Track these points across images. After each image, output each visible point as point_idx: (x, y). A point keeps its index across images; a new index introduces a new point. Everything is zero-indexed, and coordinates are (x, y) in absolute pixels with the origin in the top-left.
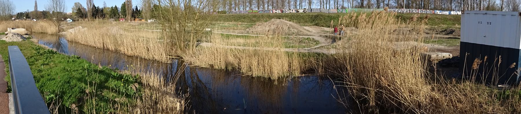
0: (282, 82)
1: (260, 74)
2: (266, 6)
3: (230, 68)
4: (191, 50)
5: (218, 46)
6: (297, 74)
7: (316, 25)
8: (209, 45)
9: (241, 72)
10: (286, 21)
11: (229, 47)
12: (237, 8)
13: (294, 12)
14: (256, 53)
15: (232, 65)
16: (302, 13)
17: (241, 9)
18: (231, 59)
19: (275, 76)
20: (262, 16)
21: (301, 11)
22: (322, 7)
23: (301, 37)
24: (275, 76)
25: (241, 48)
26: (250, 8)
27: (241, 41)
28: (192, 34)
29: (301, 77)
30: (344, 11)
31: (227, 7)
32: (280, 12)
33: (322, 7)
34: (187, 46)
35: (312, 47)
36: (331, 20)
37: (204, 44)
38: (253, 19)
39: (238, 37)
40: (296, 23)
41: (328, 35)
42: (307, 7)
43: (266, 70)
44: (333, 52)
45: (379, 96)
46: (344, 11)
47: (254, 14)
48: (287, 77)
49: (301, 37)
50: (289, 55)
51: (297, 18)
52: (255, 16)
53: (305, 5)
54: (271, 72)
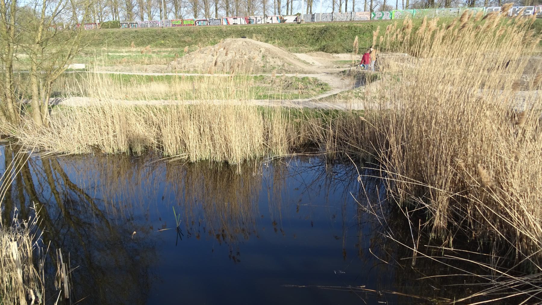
0: (251, 169)
1: (205, 155)
2: (212, 9)
3: (139, 149)
4: (38, 117)
5: (105, 102)
6: (281, 152)
7: (323, 49)
8: (83, 101)
9: (166, 154)
10: (259, 43)
11: (131, 103)
12: (145, 16)
13: (275, 21)
14: (193, 113)
15: (143, 141)
16: (291, 25)
17: (156, 18)
18: (140, 129)
19: (236, 158)
20: (205, 31)
21: (290, 19)
22: (337, 9)
23: (290, 75)
24: (236, 158)
25: (158, 104)
26: (176, 14)
27: (160, 88)
28: (34, 80)
29: (289, 158)
30: (386, 16)
31: (122, 15)
32: (243, 22)
33: (337, 9)
34: (24, 109)
35: (314, 98)
36: (354, 35)
37: (70, 102)
38: (185, 38)
39: (150, 79)
40: (280, 46)
41: (346, 68)
42: (303, 11)
43: (218, 146)
44: (357, 105)
45: (458, 205)
46: (386, 16)
47: (186, 28)
48: (261, 158)
49: (290, 75)
50: (264, 113)
51: (286, 35)
52: (188, 33)
53: (300, 7)
54: (229, 150)
